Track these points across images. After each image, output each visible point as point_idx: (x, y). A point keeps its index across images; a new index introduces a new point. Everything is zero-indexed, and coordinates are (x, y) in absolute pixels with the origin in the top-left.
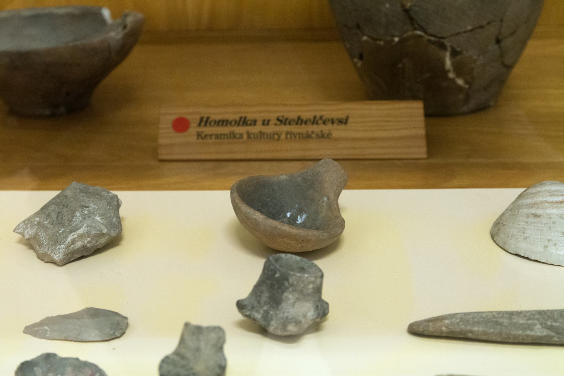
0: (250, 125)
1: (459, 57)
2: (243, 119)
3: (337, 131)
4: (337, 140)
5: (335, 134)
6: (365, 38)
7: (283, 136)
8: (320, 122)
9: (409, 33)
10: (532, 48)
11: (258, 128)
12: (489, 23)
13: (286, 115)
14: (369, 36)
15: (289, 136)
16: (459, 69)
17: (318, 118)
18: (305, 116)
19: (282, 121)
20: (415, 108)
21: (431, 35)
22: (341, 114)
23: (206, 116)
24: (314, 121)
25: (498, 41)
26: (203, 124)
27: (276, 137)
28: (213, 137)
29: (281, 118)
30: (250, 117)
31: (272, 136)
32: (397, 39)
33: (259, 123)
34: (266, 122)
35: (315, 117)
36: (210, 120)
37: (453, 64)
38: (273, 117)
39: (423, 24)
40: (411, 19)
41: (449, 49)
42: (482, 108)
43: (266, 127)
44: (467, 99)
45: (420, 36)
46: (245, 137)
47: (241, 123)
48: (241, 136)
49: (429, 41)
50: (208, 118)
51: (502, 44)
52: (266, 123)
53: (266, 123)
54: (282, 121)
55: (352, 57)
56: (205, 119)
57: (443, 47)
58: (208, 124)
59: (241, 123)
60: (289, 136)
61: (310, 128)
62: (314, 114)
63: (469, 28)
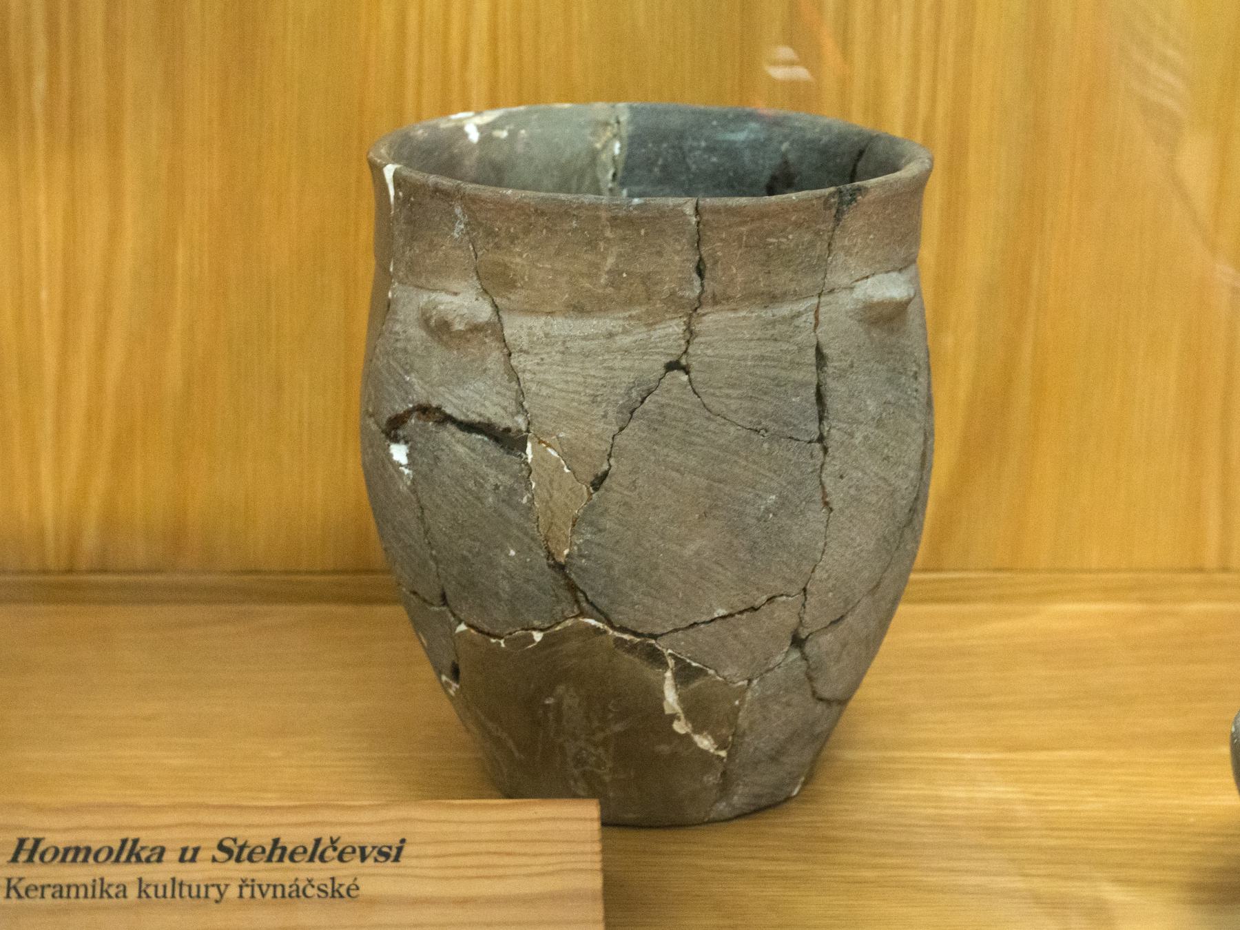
0: (148, 860)
1: (696, 684)
2: (129, 845)
3: (376, 880)
4: (373, 902)
5: (368, 887)
6: (462, 627)
7: (233, 892)
8: (330, 853)
9: (569, 623)
10: (913, 627)
11: (157, 873)
12: (770, 600)
13: (243, 835)
14: (470, 626)
15: (247, 892)
16: (696, 710)
17: (326, 842)
18: (291, 839)
19: (231, 851)
20: (581, 818)
21: (624, 630)
22: (386, 836)
23: (32, 835)
24: (316, 853)
25: (798, 642)
26: (23, 857)
27: (213, 893)
28: (48, 892)
29: (228, 843)
30: (148, 839)
31: (203, 890)
32: (538, 636)
33: (171, 856)
34: (189, 855)
35: (318, 841)
36: (41, 848)
37: (682, 699)
38: (208, 839)
39: (602, 602)
40: (572, 588)
41: (671, 662)
42: (766, 806)
43: (189, 866)
44: (725, 787)
45: (597, 630)
46: (133, 892)
47: (124, 857)
48: (123, 890)
49: (619, 642)
50: (37, 842)
51: (808, 648)
52: (189, 855)
53: (189, 855)
54: (231, 851)
55: (439, 673)
56: (29, 845)
57: (655, 657)
58: (36, 858)
59: (124, 857)
60: (247, 892)
61: (304, 871)
62: (315, 832)
63: (722, 612)
